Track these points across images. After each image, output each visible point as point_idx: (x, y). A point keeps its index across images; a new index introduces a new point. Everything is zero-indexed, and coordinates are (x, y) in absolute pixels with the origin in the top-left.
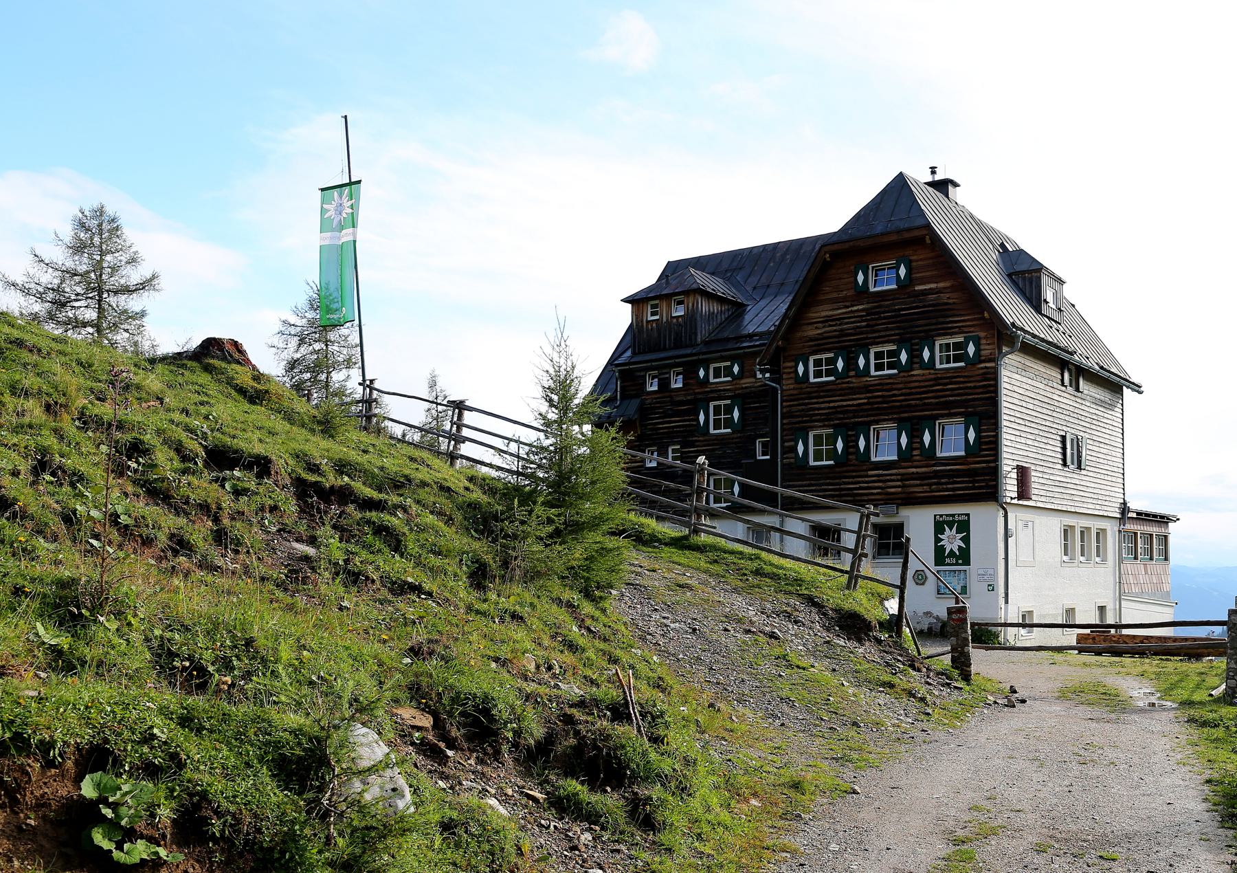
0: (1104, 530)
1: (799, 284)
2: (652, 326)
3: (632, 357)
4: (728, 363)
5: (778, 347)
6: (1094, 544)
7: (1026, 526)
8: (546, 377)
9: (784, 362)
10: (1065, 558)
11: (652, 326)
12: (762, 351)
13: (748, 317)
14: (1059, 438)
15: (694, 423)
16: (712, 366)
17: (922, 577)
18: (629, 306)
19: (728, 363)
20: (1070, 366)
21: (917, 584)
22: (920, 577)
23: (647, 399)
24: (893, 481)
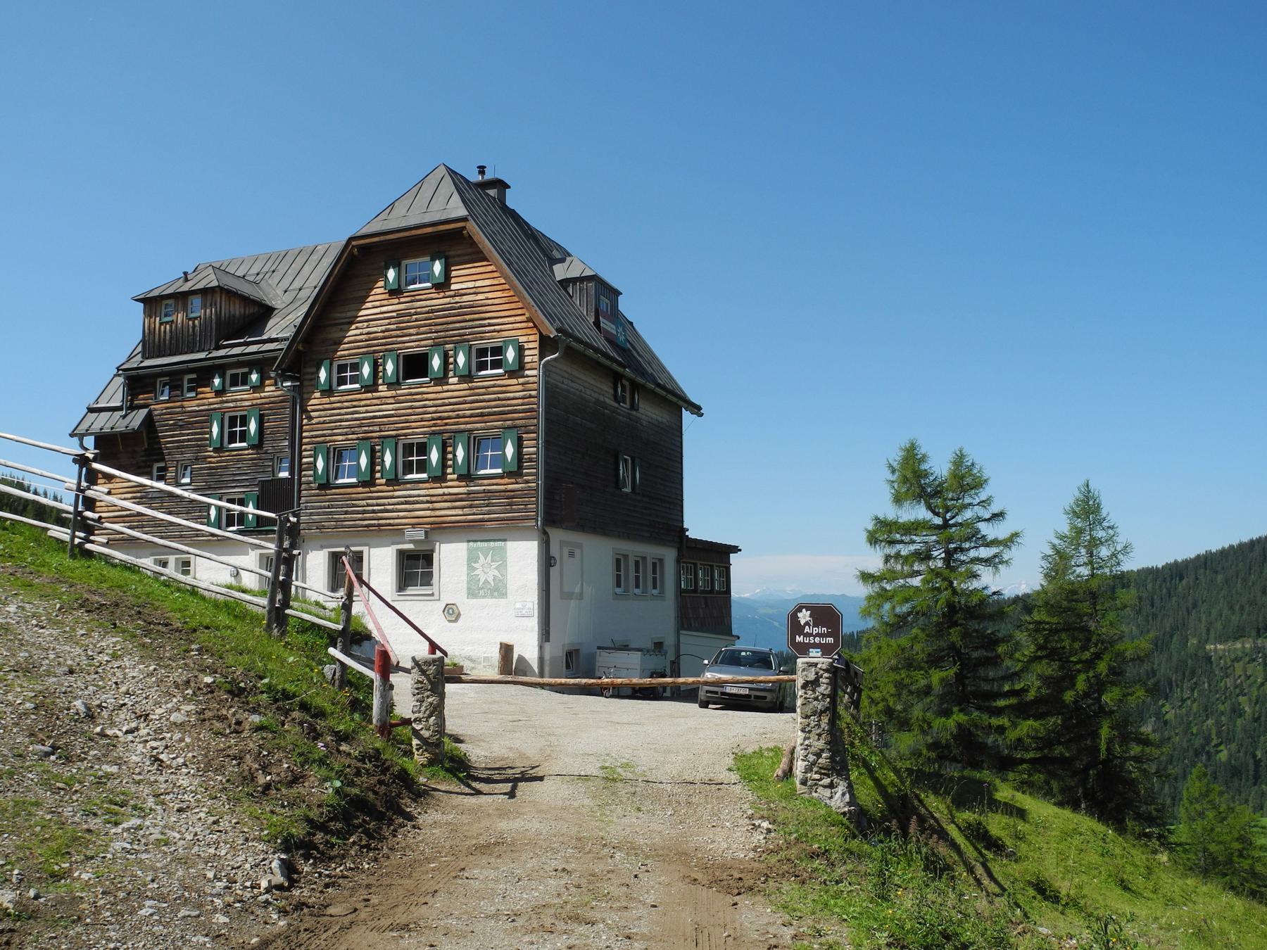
0: (661, 561)
1: (317, 289)
2: (194, 323)
3: (142, 362)
4: (246, 370)
5: (297, 351)
6: (632, 574)
7: (572, 554)
8: (995, 525)
9: (305, 367)
10: (618, 590)
11: (194, 323)
12: (276, 358)
13: (271, 323)
14: (313, 414)
15: (207, 436)
16: (229, 373)
17: (453, 611)
18: (142, 305)
19: (246, 370)
20: (625, 383)
21: (450, 621)
22: (451, 611)
23: (155, 410)
24: (422, 502)
